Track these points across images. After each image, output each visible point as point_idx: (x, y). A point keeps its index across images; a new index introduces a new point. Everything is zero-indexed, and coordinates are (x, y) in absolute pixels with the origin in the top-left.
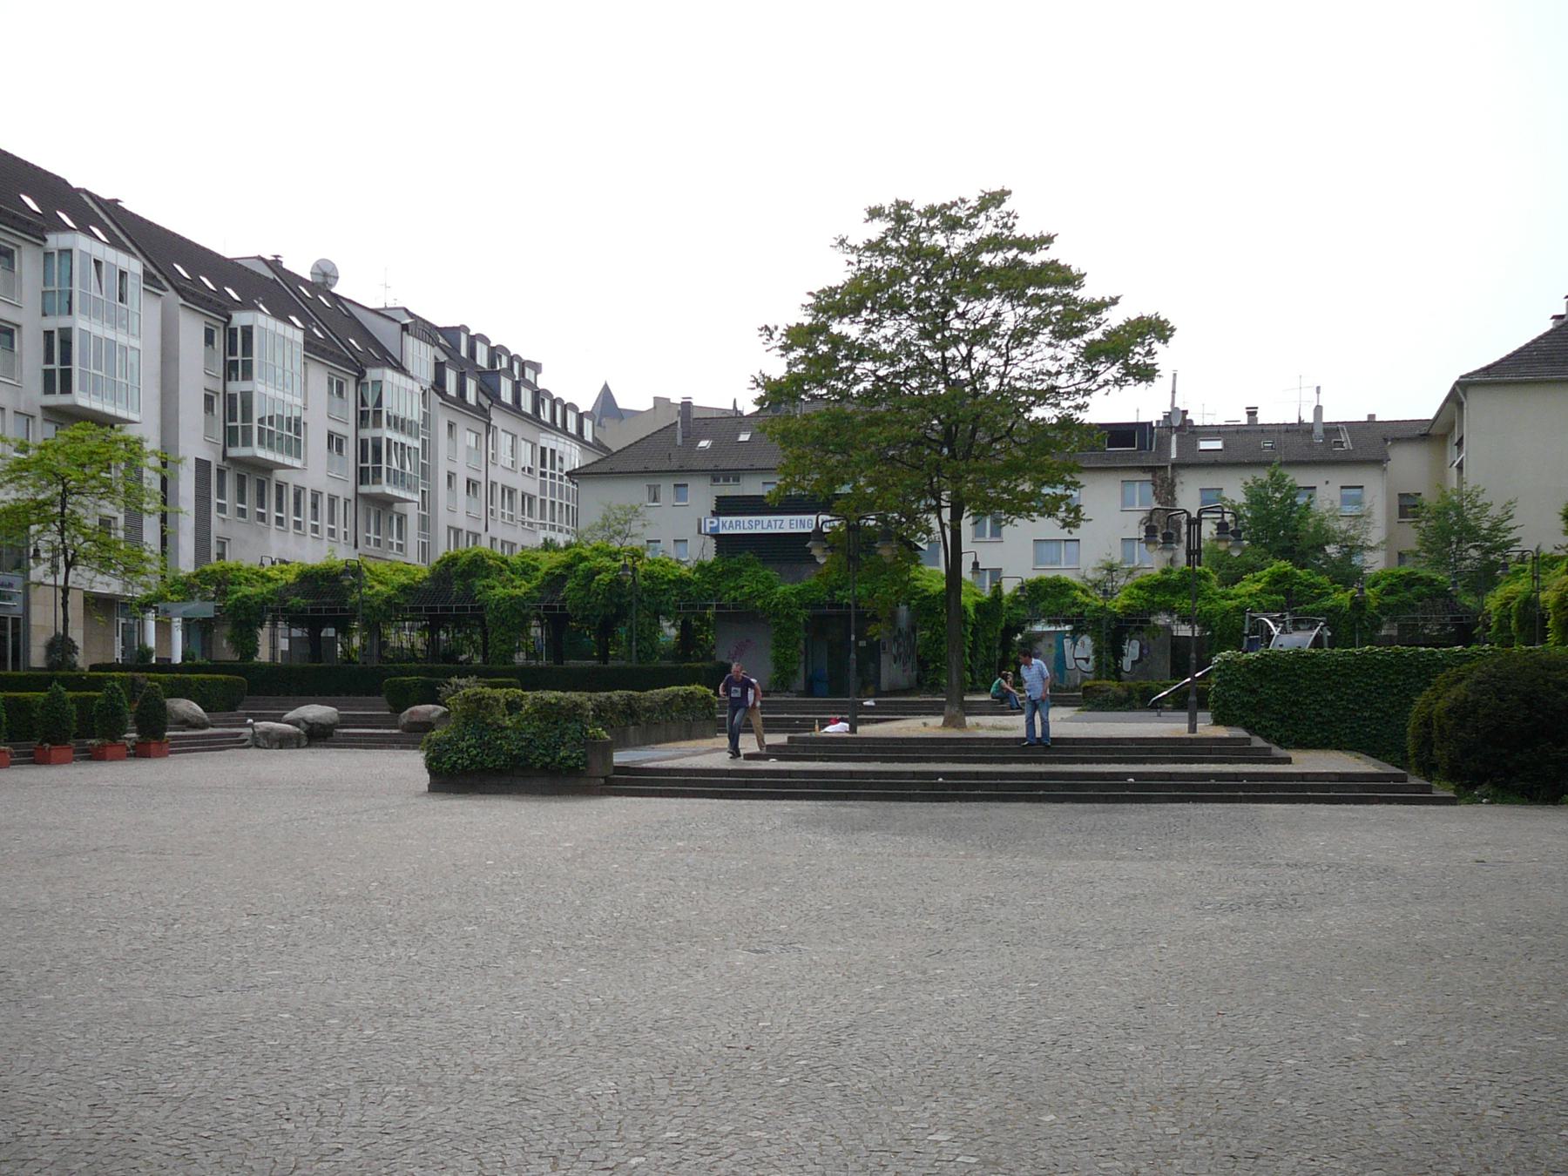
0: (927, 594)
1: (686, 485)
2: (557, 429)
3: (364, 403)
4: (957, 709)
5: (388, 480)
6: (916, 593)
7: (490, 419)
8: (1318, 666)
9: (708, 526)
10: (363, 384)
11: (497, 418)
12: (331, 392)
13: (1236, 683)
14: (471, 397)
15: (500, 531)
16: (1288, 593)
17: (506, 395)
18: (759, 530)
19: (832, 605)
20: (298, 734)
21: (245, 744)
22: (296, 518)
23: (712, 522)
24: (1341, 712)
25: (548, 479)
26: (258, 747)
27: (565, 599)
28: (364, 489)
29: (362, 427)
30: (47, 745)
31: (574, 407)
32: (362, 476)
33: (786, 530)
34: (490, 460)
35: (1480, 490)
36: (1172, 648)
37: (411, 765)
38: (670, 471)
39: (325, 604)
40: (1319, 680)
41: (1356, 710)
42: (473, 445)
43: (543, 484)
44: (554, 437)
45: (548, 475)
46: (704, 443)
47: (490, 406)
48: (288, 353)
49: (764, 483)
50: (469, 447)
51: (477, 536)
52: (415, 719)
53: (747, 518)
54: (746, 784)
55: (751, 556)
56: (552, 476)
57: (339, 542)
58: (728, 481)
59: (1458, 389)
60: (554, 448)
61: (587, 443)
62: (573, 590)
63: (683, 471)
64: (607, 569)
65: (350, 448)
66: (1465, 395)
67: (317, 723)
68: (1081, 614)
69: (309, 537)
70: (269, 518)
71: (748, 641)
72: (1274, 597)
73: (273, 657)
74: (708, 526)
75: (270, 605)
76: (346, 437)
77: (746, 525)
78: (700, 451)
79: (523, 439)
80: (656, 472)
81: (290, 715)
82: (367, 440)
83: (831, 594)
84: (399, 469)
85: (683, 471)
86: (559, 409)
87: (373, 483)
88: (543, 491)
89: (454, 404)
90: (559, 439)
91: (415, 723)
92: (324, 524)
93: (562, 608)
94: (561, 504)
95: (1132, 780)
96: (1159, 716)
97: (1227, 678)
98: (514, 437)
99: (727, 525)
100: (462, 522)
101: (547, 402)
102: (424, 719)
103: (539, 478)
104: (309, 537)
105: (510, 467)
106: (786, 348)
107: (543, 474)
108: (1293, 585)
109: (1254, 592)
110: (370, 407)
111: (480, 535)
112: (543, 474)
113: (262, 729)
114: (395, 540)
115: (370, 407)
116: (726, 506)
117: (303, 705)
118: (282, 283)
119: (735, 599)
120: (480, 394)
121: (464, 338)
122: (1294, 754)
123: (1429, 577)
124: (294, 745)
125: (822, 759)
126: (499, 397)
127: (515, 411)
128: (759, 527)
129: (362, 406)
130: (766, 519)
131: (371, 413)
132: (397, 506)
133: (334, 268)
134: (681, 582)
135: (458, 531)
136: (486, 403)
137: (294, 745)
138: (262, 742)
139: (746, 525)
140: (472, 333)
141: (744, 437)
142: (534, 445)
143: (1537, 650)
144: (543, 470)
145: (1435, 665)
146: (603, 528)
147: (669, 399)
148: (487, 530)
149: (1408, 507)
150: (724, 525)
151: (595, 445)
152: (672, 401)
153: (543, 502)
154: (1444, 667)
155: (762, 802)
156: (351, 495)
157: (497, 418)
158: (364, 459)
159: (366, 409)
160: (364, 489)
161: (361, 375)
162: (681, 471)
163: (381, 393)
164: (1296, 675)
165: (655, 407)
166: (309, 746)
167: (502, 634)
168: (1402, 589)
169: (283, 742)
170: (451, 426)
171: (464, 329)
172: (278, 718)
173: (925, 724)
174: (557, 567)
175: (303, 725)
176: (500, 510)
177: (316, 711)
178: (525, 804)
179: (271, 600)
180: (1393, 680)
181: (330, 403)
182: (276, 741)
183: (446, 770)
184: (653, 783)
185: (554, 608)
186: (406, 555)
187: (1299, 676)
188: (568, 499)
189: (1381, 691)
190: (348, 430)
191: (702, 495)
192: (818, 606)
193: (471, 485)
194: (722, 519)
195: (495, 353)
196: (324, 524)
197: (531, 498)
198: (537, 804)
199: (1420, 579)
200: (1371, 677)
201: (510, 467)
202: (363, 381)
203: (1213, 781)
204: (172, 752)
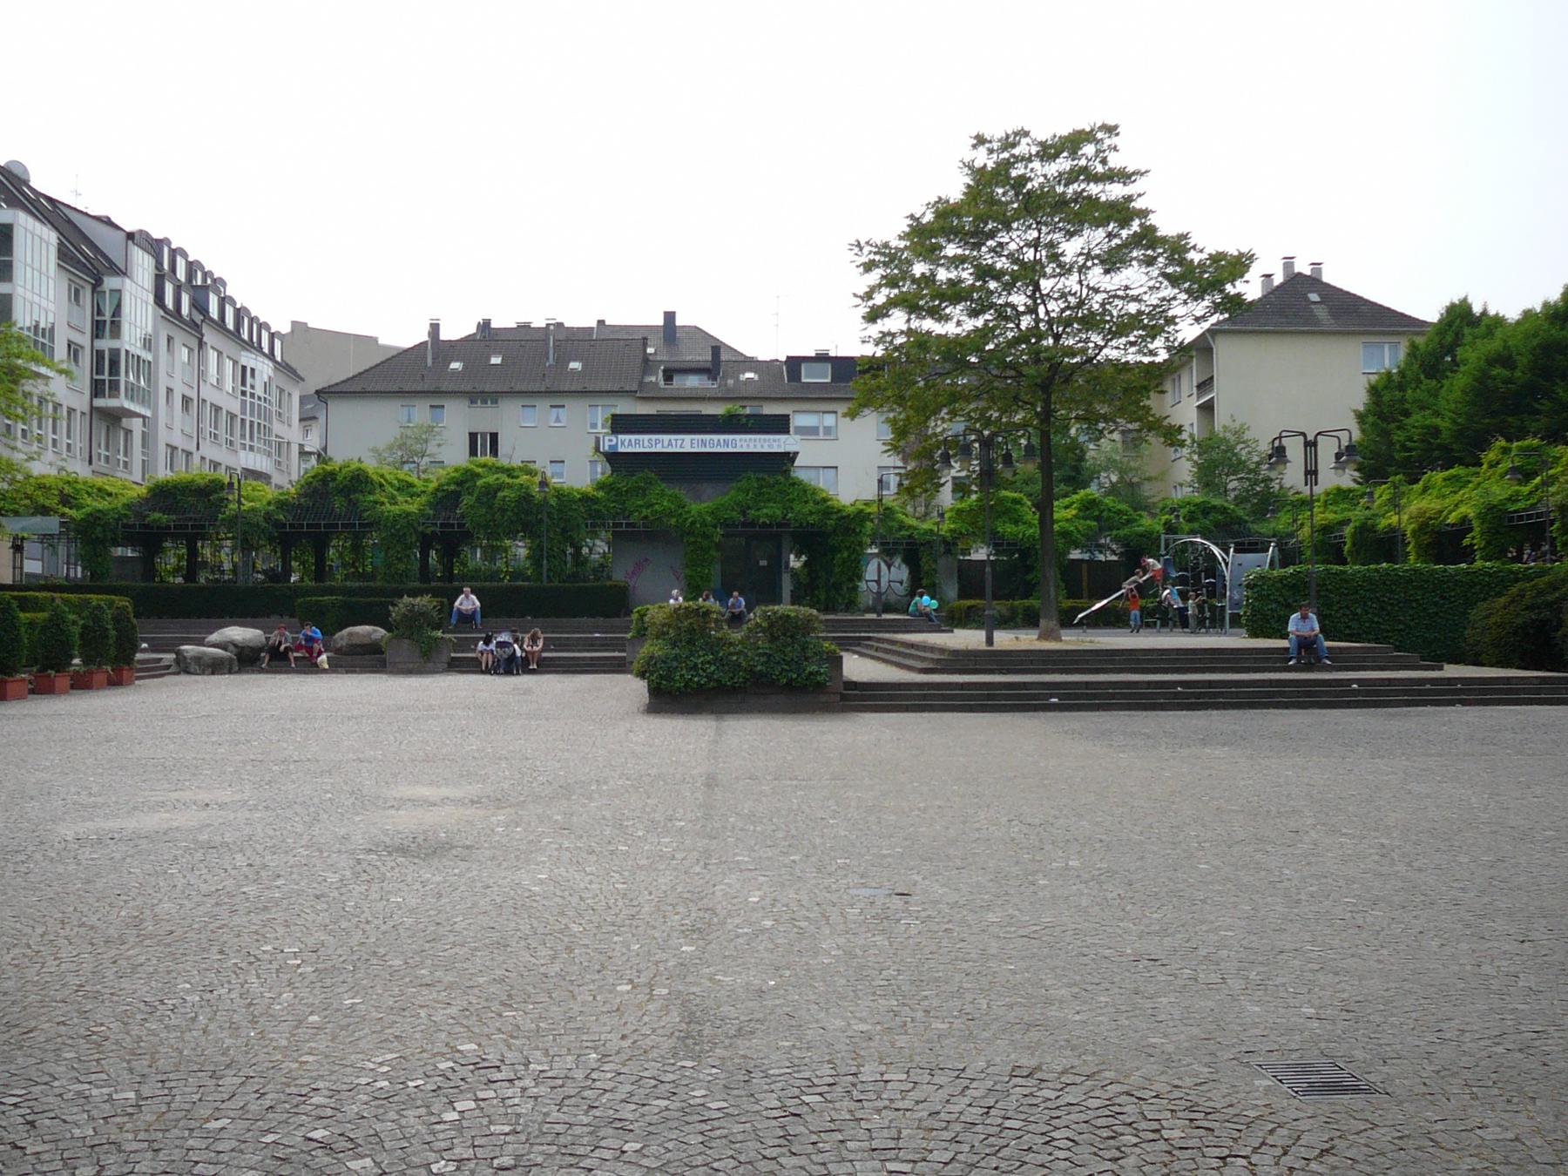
0: (844, 514)
1: (443, 406)
2: (253, 347)
3: (100, 313)
5: (126, 396)
6: (832, 513)
7: (202, 335)
8: (1346, 582)
9: (607, 444)
11: (210, 336)
14: (185, 310)
15: (210, 451)
16: (1098, 519)
17: (214, 312)
18: (659, 449)
19: (744, 524)
20: (230, 659)
22: (39, 432)
23: (611, 440)
24: (1367, 625)
25: (248, 399)
26: (188, 673)
27: (463, 516)
28: (100, 402)
29: (97, 337)
31: (266, 326)
32: (97, 389)
33: (687, 449)
34: (201, 375)
35: (1246, 427)
37: (633, 688)
40: (1347, 595)
42: (186, 360)
43: (243, 403)
44: (254, 356)
45: (248, 394)
46: (455, 365)
47: (202, 321)
48: (44, 252)
49: (431, 406)
50: (184, 363)
51: (189, 454)
52: (356, 641)
53: (646, 437)
54: (989, 697)
56: (252, 395)
57: (75, 458)
59: (1207, 335)
63: (366, 392)
64: (510, 486)
65: (86, 359)
69: (50, 451)
70: (16, 431)
72: (1088, 522)
73: (14, 581)
74: (607, 444)
75: (125, 521)
76: (82, 347)
77: (646, 443)
78: (453, 373)
79: (228, 357)
81: (215, 637)
82: (104, 351)
83: (744, 513)
84: (135, 382)
85: (366, 392)
86: (255, 326)
87: (109, 397)
88: (243, 412)
90: (259, 358)
92: (222, 432)
94: (259, 424)
95: (1056, 700)
98: (220, 353)
99: (626, 444)
100: (178, 441)
101: (246, 320)
102: (366, 641)
105: (215, 384)
107: (244, 393)
108: (1102, 512)
109: (1069, 517)
110: (107, 317)
111: (191, 453)
112: (244, 393)
114: (121, 457)
115: (107, 317)
116: (621, 424)
117: (227, 626)
118: (11, 188)
119: (646, 517)
120: (194, 311)
121: (166, 250)
122: (1446, 666)
123: (1222, 506)
124: (226, 671)
126: (208, 312)
127: (220, 327)
128: (659, 446)
130: (666, 438)
132: (125, 422)
134: (586, 499)
135: (174, 448)
136: (198, 318)
137: (226, 671)
138: (193, 667)
139: (646, 443)
140: (173, 246)
141: (496, 360)
142: (235, 363)
143: (1531, 568)
145: (1448, 581)
146: (400, 447)
147: (306, 324)
148: (198, 449)
150: (622, 443)
153: (243, 420)
154: (1517, 580)
156: (86, 409)
157: (210, 336)
158: (100, 371)
159: (103, 318)
160: (100, 402)
161: (98, 283)
162: (437, 393)
164: (1327, 590)
165: (292, 331)
166: (239, 672)
167: (398, 552)
168: (1200, 516)
169: (215, 667)
170: (170, 339)
171: (166, 241)
172: (201, 643)
173: (1017, 638)
174: (448, 484)
175: (231, 648)
176: (209, 429)
177: (238, 633)
180: (1411, 595)
181: (70, 313)
182: (209, 666)
183: (679, 688)
184: (891, 698)
186: (131, 473)
188: (259, 417)
189: (1401, 605)
190: (84, 340)
191: (599, 415)
193: (186, 401)
194: (621, 437)
195: (192, 267)
196: (222, 432)
197: (232, 416)
198: (791, 723)
199: (1214, 507)
200: (1392, 592)
202: (99, 289)
203: (1428, 686)
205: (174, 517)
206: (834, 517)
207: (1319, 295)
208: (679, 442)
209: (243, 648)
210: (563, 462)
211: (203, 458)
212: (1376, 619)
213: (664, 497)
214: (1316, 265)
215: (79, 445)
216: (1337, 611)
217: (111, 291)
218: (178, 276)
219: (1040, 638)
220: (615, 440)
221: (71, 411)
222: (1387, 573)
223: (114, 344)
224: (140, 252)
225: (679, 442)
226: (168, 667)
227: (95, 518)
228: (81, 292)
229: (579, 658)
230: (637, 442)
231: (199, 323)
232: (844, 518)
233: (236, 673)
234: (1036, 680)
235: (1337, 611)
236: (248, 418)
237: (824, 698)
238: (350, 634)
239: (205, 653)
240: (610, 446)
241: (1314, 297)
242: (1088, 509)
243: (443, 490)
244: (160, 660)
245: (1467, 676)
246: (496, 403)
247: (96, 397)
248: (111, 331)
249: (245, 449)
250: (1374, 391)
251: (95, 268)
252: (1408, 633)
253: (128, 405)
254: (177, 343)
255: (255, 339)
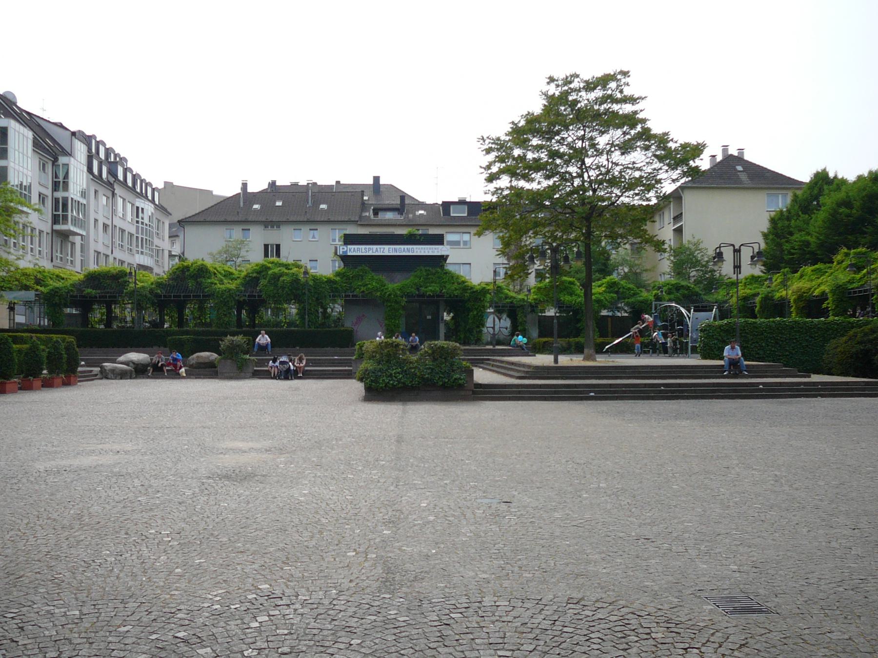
0: (474, 290)
1: (249, 230)
3: (56, 177)
4: (593, 351)
7: (114, 189)
9: (341, 250)
10: (56, 165)
11: (118, 190)
12: (40, 170)
13: (715, 337)
14: (104, 175)
17: (121, 177)
20: (131, 371)
21: (97, 377)
23: (343, 249)
24: (768, 352)
25: (140, 225)
27: (260, 291)
28: (57, 227)
29: (55, 190)
30: (31, 378)
31: (150, 184)
32: (55, 220)
34: (114, 212)
36: (539, 322)
37: (356, 387)
38: (238, 221)
39: (108, 292)
40: (757, 335)
41: (776, 352)
42: (105, 204)
43: (137, 227)
44: (143, 201)
45: (140, 223)
47: (114, 182)
48: (25, 143)
50: (104, 205)
51: (107, 256)
52: (201, 361)
53: (363, 247)
54: (555, 392)
55: (367, 268)
56: (142, 223)
57: (43, 258)
58: (274, 228)
59: (679, 189)
60: (138, 206)
61: (156, 205)
62: (266, 286)
63: (206, 222)
64: (287, 274)
65: (49, 203)
66: (683, 193)
67: (141, 364)
68: (511, 303)
69: (29, 255)
71: (363, 316)
72: (612, 295)
73: (9, 327)
74: (341, 250)
77: (363, 250)
78: (255, 211)
79: (129, 202)
80: (215, 222)
81: (122, 358)
82: (59, 198)
83: (418, 289)
85: (206, 222)
86: (144, 184)
87: (62, 224)
88: (137, 232)
89: (97, 179)
91: (201, 363)
93: (260, 296)
94: (146, 239)
96: (609, 356)
97: (711, 334)
98: (124, 200)
99: (352, 250)
100: (101, 249)
101: (139, 181)
103: (135, 224)
104: (29, 255)
105: (122, 217)
106: (488, 151)
107: (137, 222)
108: (619, 289)
110: (61, 179)
111: (108, 256)
112: (137, 222)
113: (109, 368)
114: (69, 258)
115: (61, 179)
116: (349, 239)
119: (363, 292)
120: (109, 176)
123: (687, 285)
125: (562, 378)
126: (117, 176)
128: (371, 251)
129: (56, 178)
131: (61, 183)
132: (71, 238)
133: (14, 97)
134: (329, 281)
135: (99, 253)
136: (112, 180)
137: (129, 377)
139: (363, 250)
140: (98, 140)
142: (133, 205)
144: (137, 219)
147: (172, 183)
148: (112, 253)
149: (666, 249)
150: (350, 250)
151: (160, 206)
152: (174, 184)
154: (853, 327)
155: (539, 402)
156: (49, 231)
157: (118, 190)
158: (57, 209)
160: (57, 227)
161: (56, 160)
162: (246, 222)
163: (68, 170)
164: (746, 332)
165: (165, 187)
169: (122, 375)
170: (96, 192)
171: (94, 137)
172: (114, 361)
174: (252, 273)
175: (131, 364)
177: (135, 356)
178: (389, 406)
179: (72, 290)
181: (40, 177)
185: (255, 296)
186: (75, 267)
187: (747, 333)
189: (787, 341)
190: (48, 192)
192: (412, 296)
193: (105, 226)
195: (108, 151)
196: (126, 246)
197: (131, 235)
199: (682, 286)
201: (122, 217)
202: (56, 164)
203: (802, 387)
204: (80, 381)
205: (99, 291)
206: (469, 291)
207: (743, 167)
208: (382, 250)
209: (138, 364)
210: (317, 261)
211: (115, 259)
212: (773, 349)
213: (373, 280)
214: (741, 150)
215: (45, 251)
216: (751, 344)
217: (63, 165)
218: (101, 156)
219: (584, 359)
220: (346, 248)
221: (41, 232)
222: (779, 323)
223: (65, 194)
224: (79, 143)
225: (382, 250)
226: (96, 375)
227: (55, 292)
228: (46, 165)
229: (325, 370)
230: (358, 250)
231: (112, 182)
232: (474, 292)
233: (134, 378)
234: (531, 380)
235: (751, 344)
236: (140, 236)
237: (463, 393)
238: (198, 357)
239: (116, 367)
240: (343, 252)
241: (740, 168)
242: (611, 287)
243: (250, 277)
244: (91, 371)
245: (824, 381)
246: (279, 227)
247: (55, 224)
248: (63, 187)
249: (138, 253)
250: (773, 221)
251: (54, 152)
252: (791, 357)
253: (73, 228)
254: (100, 193)
255: (144, 192)
